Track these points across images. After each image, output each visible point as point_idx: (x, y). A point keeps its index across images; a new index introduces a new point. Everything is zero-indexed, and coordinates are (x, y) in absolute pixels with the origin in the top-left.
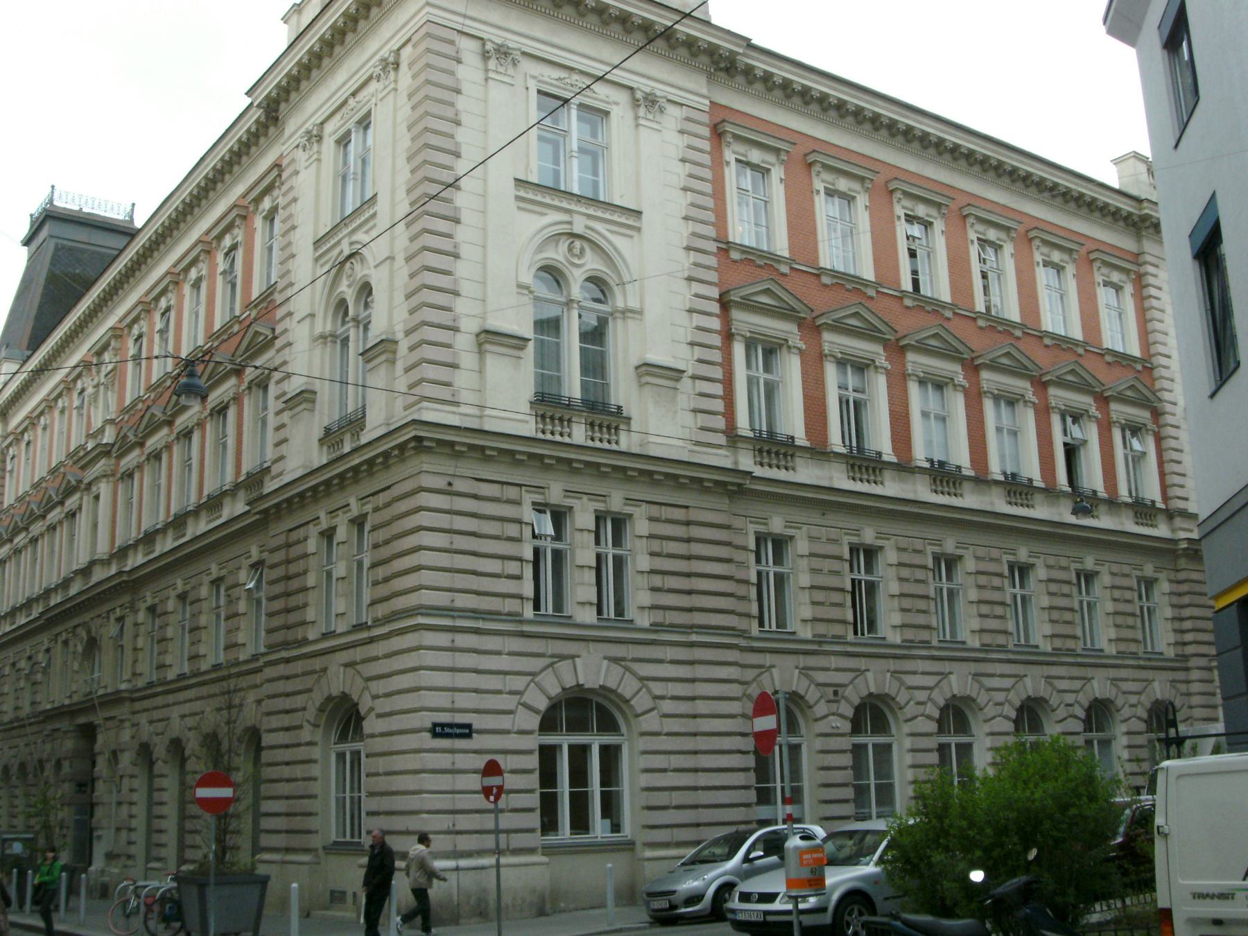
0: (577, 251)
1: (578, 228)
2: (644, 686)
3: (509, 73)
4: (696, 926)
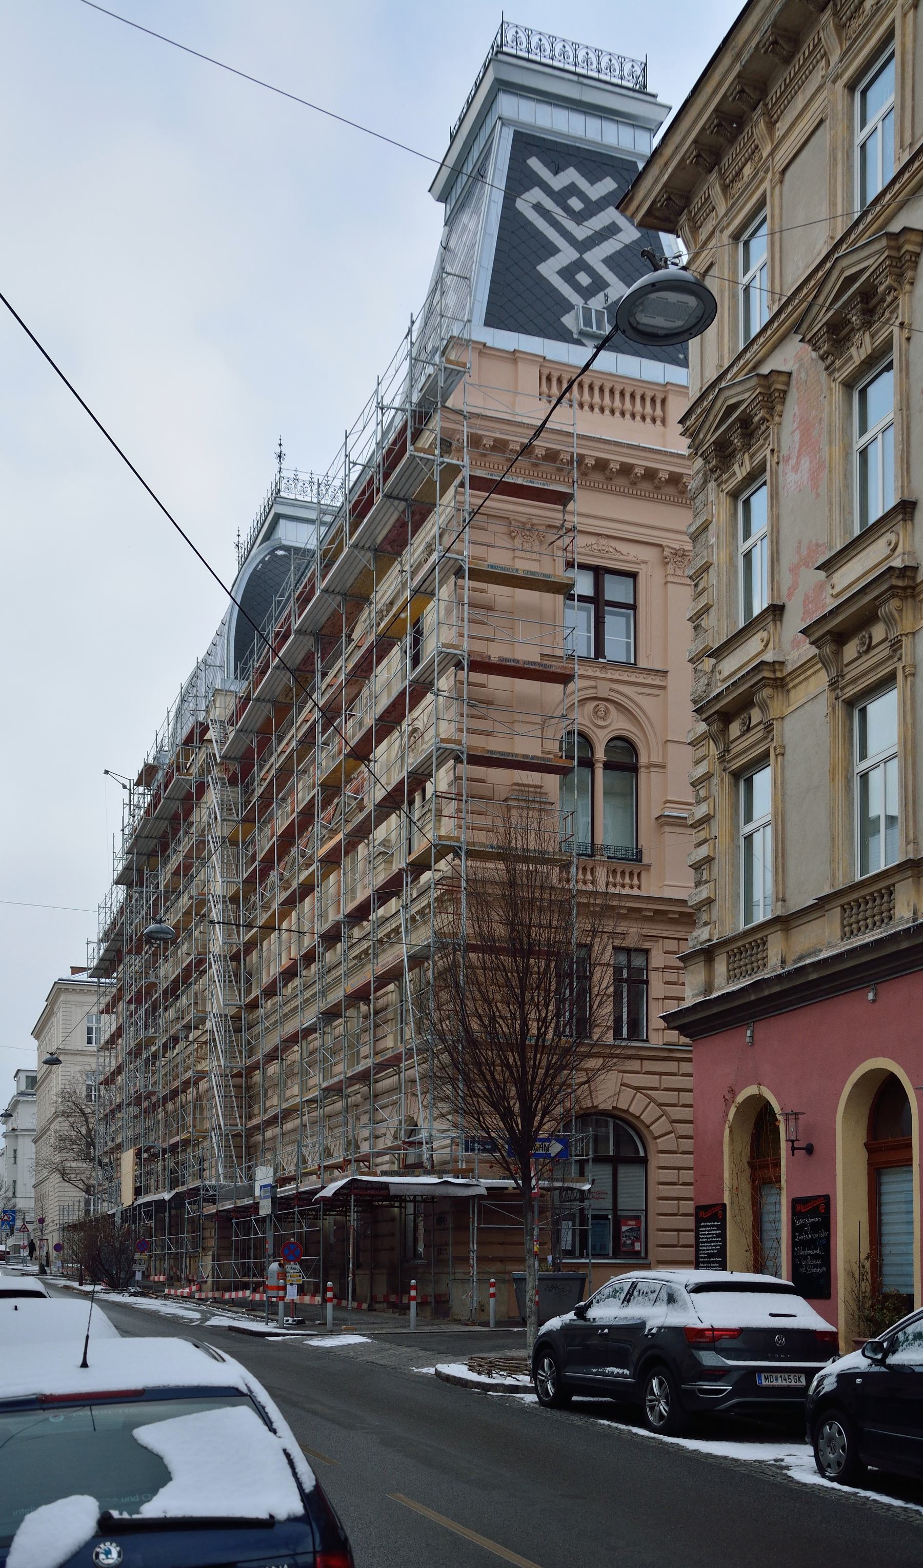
0: (601, 714)
1: (603, 690)
2: (664, 1114)
3: (535, 549)
4: (209, 1385)
